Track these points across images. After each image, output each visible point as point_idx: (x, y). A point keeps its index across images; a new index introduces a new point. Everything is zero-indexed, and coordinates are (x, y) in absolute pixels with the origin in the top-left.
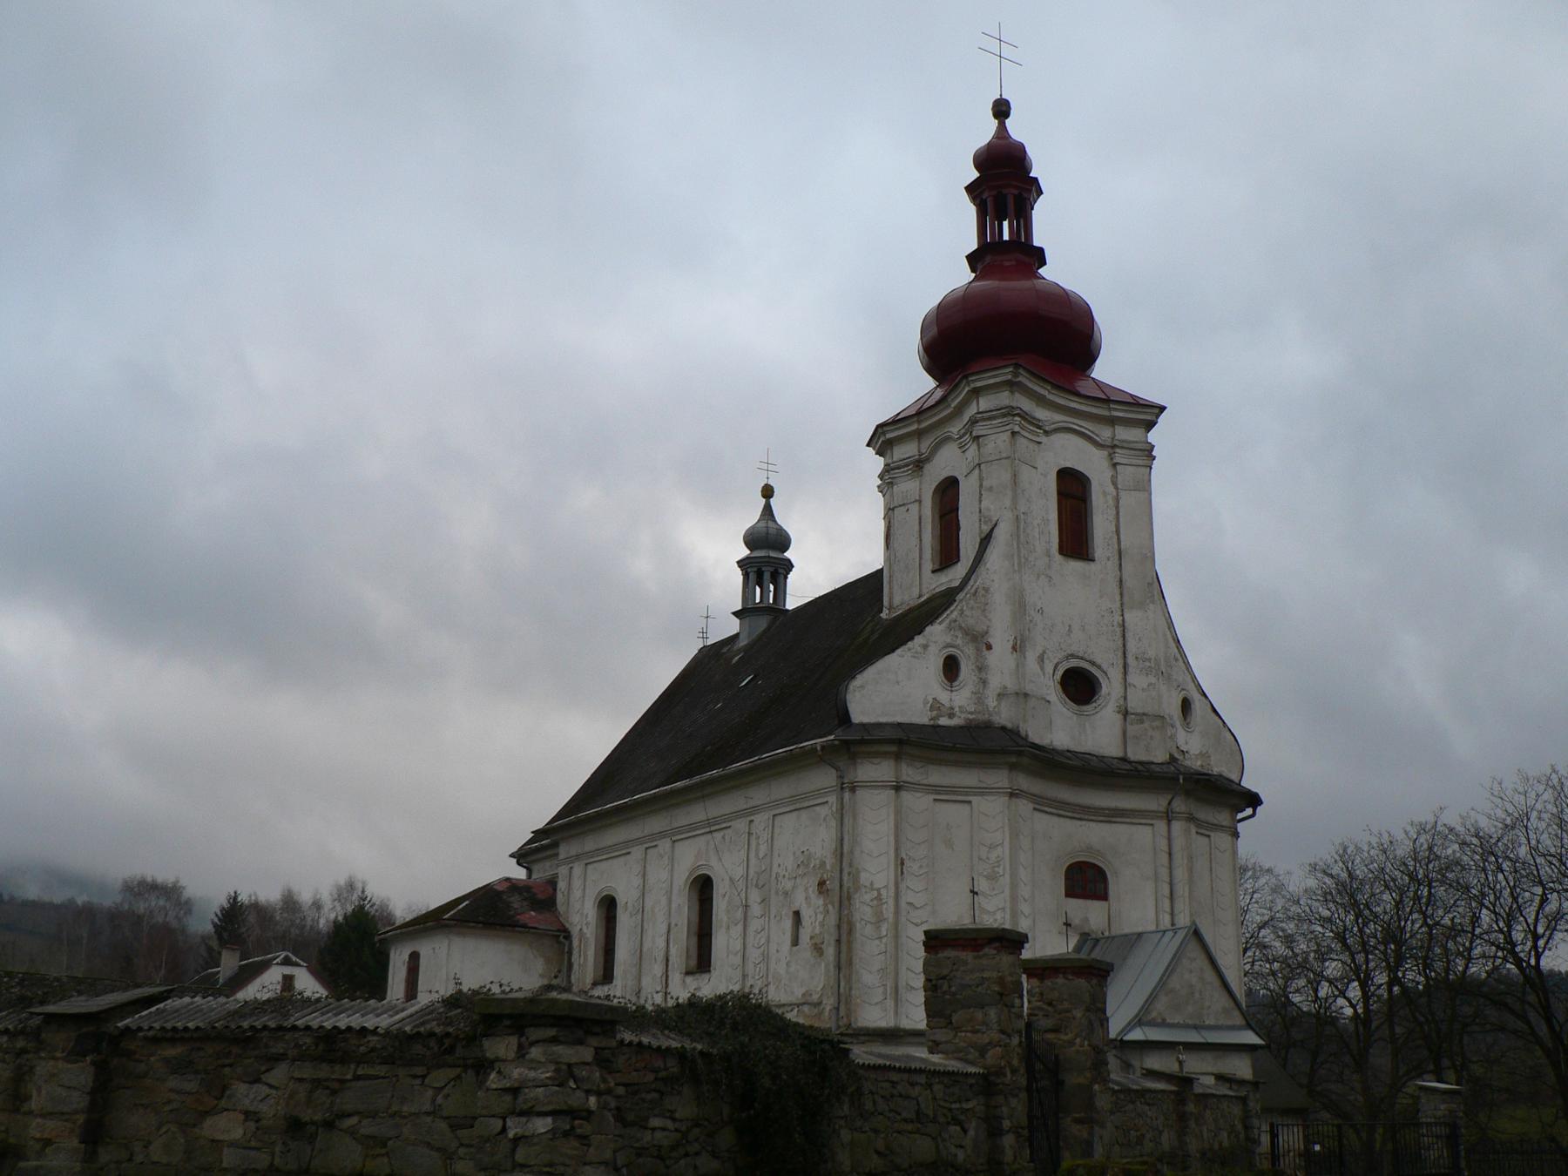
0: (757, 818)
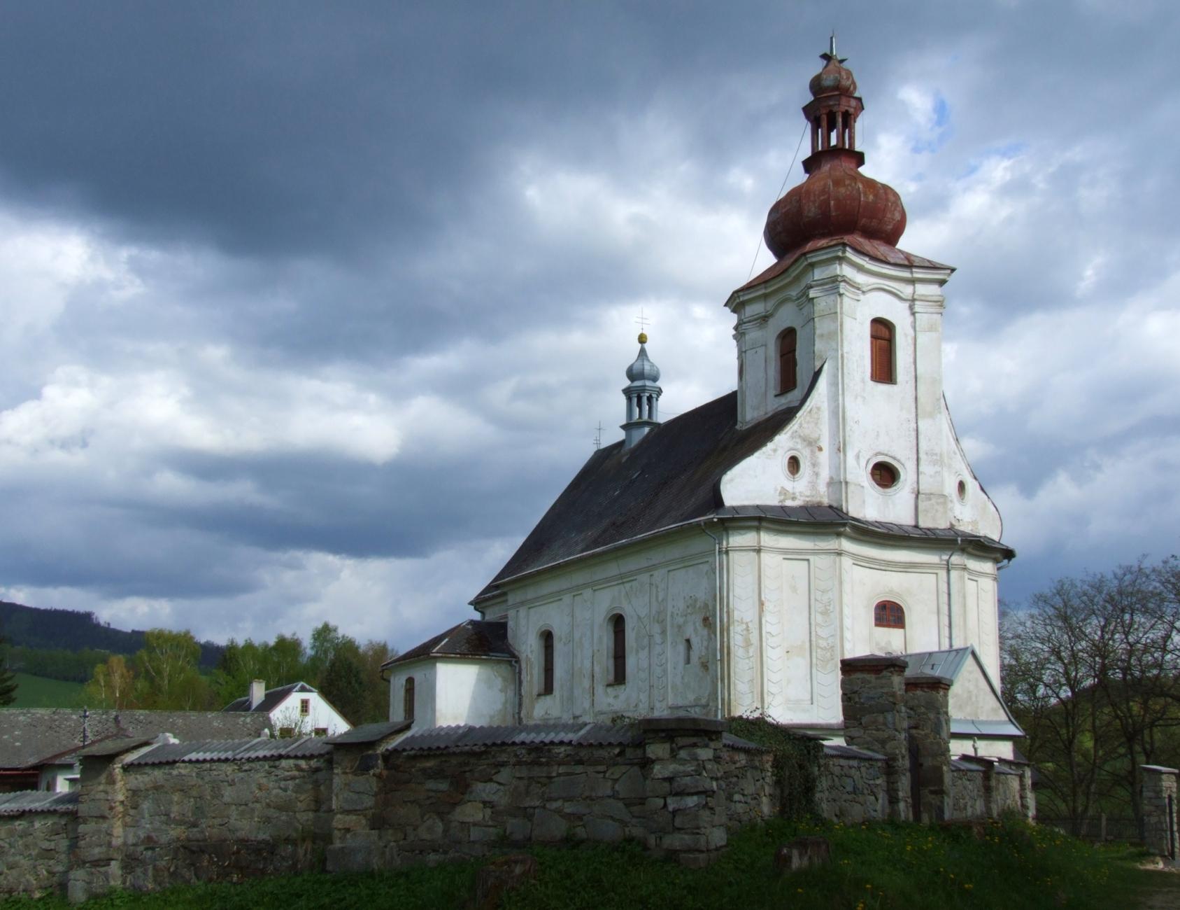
0: (656, 573)
